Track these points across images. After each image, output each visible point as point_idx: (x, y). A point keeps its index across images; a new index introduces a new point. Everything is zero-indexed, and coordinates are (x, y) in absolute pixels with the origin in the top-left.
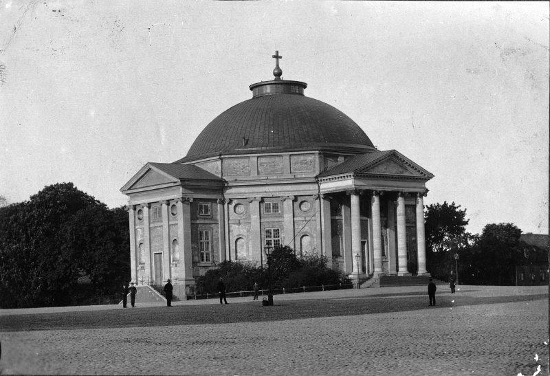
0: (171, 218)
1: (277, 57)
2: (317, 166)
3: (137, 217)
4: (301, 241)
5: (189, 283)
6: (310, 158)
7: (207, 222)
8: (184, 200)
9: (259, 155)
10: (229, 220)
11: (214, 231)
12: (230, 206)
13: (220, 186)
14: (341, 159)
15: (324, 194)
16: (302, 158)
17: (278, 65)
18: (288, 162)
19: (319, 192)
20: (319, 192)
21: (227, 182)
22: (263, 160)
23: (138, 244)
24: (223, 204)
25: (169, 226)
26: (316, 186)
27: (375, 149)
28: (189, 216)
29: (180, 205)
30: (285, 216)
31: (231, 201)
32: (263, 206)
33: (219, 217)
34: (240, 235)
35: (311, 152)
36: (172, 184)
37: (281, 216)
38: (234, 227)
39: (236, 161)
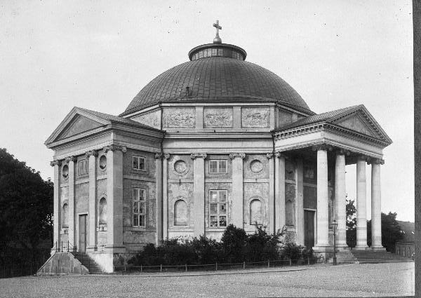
0: (99, 172)
1: (216, 26)
2: (272, 121)
3: (62, 173)
4: (175, 205)
5: (119, 251)
6: (263, 112)
7: (142, 178)
8: (115, 148)
9: (205, 104)
10: (168, 178)
11: (150, 191)
12: (170, 163)
13: (161, 137)
14: (295, 118)
15: (282, 153)
16: (255, 111)
17: (217, 34)
18: (239, 114)
19: (274, 150)
20: (274, 150)
21: (169, 134)
22: (211, 111)
23: (62, 205)
24: (162, 160)
25: (97, 181)
26: (269, 144)
27: (313, 114)
28: (120, 169)
29: (110, 155)
30: (234, 176)
31: (172, 155)
32: (208, 163)
33: (157, 175)
34: (180, 197)
35: (266, 104)
36: (101, 129)
37: (229, 176)
38: (174, 188)
39: (178, 111)
